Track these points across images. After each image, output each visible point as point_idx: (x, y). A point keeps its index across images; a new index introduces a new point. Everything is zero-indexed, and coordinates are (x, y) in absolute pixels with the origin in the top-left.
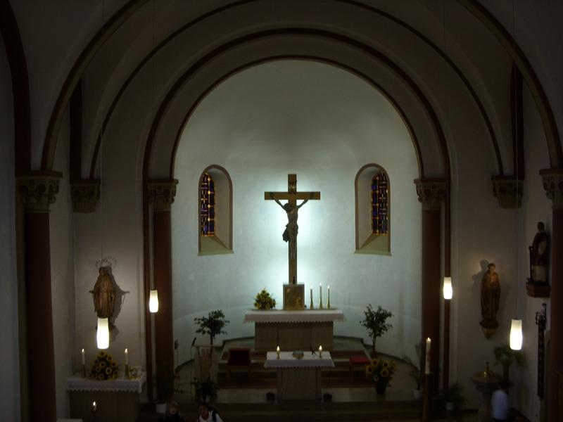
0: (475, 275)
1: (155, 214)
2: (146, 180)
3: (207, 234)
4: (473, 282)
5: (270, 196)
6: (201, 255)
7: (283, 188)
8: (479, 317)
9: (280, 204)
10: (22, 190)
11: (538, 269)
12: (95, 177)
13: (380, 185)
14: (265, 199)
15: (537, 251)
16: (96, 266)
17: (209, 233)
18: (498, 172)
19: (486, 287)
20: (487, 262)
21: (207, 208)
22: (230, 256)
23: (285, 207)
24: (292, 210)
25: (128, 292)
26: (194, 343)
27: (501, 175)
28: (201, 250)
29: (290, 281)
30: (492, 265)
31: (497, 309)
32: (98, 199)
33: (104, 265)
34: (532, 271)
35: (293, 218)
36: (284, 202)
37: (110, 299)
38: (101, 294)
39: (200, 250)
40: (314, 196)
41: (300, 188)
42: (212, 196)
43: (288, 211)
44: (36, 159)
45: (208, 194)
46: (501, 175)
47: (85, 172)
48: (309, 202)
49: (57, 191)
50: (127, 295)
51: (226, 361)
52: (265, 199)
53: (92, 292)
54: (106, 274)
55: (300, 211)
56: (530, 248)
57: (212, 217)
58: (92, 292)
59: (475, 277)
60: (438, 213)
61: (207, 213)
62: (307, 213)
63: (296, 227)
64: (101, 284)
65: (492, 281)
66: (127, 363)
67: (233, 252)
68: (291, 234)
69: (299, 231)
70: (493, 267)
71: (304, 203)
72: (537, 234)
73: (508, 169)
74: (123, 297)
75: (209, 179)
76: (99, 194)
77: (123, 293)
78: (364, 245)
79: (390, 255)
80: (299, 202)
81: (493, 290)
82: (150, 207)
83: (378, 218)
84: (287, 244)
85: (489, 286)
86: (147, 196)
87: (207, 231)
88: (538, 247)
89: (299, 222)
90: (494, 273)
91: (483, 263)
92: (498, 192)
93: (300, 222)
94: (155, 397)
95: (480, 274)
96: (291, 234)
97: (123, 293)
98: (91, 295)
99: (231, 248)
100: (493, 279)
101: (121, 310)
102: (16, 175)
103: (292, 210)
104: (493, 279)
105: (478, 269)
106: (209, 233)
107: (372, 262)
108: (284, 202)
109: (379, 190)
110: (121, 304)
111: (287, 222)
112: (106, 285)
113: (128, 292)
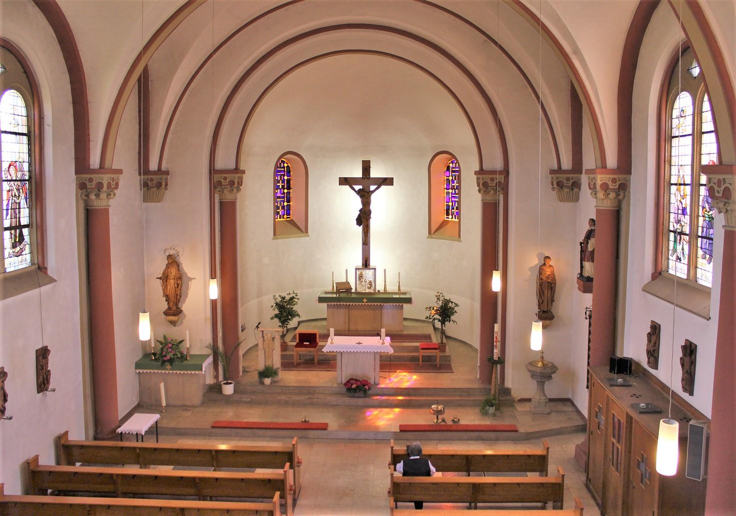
0: (531, 267)
1: (222, 203)
2: (212, 171)
3: (283, 218)
4: (529, 273)
5: (344, 181)
6: (276, 239)
7: (358, 173)
8: (536, 310)
9: (354, 189)
10: (82, 186)
11: (587, 265)
12: (164, 168)
13: (453, 171)
14: (339, 185)
15: (587, 247)
16: (165, 251)
17: (285, 216)
18: (556, 167)
19: (542, 279)
20: (542, 254)
21: (284, 193)
22: (307, 238)
23: (359, 192)
24: (365, 195)
25: (195, 279)
26: (257, 327)
27: (559, 170)
28: (276, 233)
29: (363, 265)
30: (548, 257)
31: (553, 301)
32: (166, 189)
33: (172, 252)
34: (582, 267)
35: (366, 202)
36: (357, 188)
37: (176, 286)
38: (168, 280)
39: (275, 234)
40: (388, 181)
41: (375, 173)
42: (289, 181)
43: (361, 197)
44: (95, 160)
45: (284, 180)
46: (559, 170)
47: (153, 166)
48: (383, 188)
49: (117, 187)
50: (193, 281)
51: (295, 344)
52: (339, 185)
53: (160, 278)
54: (173, 261)
55: (374, 198)
56: (581, 243)
57: (288, 201)
58: (160, 278)
59: (531, 269)
60: (495, 205)
61: (283, 197)
62: (380, 198)
63: (369, 212)
64: (169, 270)
65: (548, 273)
66: (188, 346)
67: (308, 236)
68: (364, 218)
69: (372, 216)
70: (548, 260)
71: (377, 189)
72: (589, 230)
73: (567, 164)
74: (190, 282)
75: (286, 165)
76: (166, 185)
77: (191, 279)
78: (434, 233)
79: (461, 242)
80: (372, 188)
81: (548, 282)
82: (217, 196)
83: (450, 204)
84: (360, 228)
85: (544, 278)
86: (215, 186)
87: (283, 215)
88: (588, 243)
89: (372, 207)
90: (550, 266)
91: (539, 255)
92: (555, 186)
93: (373, 207)
94: (221, 378)
95: (537, 265)
96: (364, 218)
97: (191, 279)
98: (159, 282)
99: (307, 232)
100: (548, 271)
101: (189, 296)
102: (75, 174)
103: (365, 195)
104: (548, 271)
105: (535, 261)
106: (285, 216)
107: (441, 245)
108: (357, 188)
109: (452, 176)
110: (188, 289)
111: (360, 206)
112: (173, 272)
113: (195, 279)
